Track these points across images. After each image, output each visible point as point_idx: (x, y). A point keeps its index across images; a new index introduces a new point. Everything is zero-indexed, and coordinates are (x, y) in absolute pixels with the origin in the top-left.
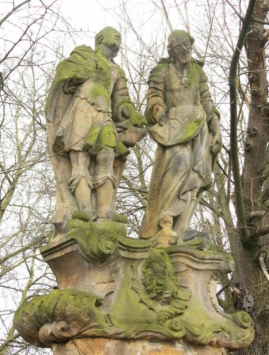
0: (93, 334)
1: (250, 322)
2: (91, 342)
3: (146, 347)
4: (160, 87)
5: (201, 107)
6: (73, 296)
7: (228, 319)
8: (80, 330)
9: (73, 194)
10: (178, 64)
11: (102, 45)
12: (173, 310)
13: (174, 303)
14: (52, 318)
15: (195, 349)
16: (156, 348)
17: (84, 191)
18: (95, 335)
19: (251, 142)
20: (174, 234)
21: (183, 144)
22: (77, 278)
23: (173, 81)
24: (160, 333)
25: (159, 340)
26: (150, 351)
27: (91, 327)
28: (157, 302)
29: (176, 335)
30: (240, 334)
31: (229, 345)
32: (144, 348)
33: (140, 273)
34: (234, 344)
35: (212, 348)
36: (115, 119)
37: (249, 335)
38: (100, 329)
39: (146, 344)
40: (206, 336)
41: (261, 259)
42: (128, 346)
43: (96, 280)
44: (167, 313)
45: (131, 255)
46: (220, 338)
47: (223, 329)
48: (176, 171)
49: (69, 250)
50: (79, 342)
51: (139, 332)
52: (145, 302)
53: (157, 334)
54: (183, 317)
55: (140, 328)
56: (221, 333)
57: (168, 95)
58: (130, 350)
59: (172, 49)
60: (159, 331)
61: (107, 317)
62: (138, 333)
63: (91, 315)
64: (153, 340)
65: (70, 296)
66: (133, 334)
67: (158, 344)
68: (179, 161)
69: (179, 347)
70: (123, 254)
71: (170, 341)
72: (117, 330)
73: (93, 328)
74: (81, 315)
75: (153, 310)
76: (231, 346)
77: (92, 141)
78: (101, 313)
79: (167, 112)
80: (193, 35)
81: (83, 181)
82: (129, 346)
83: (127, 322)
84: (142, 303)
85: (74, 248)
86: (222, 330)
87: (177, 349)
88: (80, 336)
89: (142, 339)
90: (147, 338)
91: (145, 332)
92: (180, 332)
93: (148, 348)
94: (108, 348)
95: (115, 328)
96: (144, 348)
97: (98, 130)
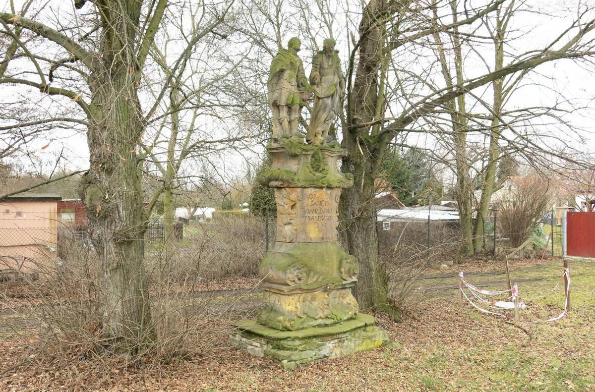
4: (318, 67)
5: (337, 76)
9: (281, 124)
10: (327, 54)
11: (292, 48)
13: (323, 172)
14: (277, 180)
17: (286, 123)
19: (358, 81)
20: (322, 138)
21: (328, 97)
22: (284, 162)
23: (325, 63)
29: (324, 186)
33: (309, 160)
34: (346, 187)
36: (298, 86)
37: (352, 183)
39: (312, 189)
40: (334, 185)
41: (357, 139)
43: (293, 164)
45: (307, 153)
48: (324, 111)
49: (281, 151)
50: (287, 189)
54: (326, 178)
57: (322, 70)
59: (325, 48)
63: (293, 180)
64: (315, 187)
68: (326, 106)
69: (325, 189)
70: (303, 153)
71: (322, 188)
77: (289, 102)
78: (296, 178)
79: (321, 79)
80: (336, 42)
81: (286, 120)
85: (284, 150)
88: (288, 187)
89: (311, 187)
97: (292, 96)
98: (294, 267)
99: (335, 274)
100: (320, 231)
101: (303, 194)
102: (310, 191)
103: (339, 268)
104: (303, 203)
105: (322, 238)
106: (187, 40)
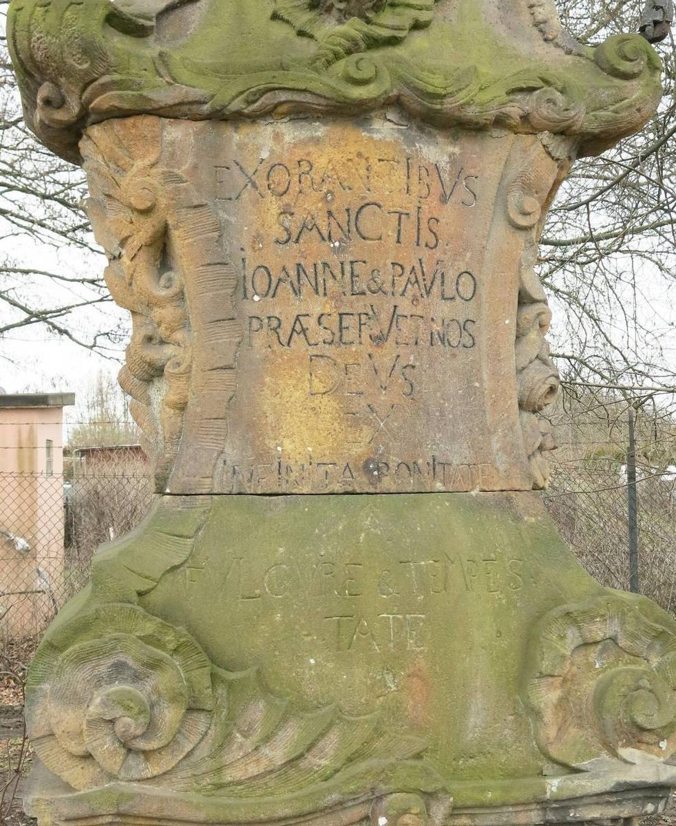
0: (112, 106)
1: (642, 59)
2: (119, 128)
3: (283, 135)
6: (42, 9)
7: (578, 58)
8: (81, 98)
12: (358, 27)
15: (455, 138)
16: (310, 135)
18: (119, 109)
24: (305, 91)
25: (319, 115)
26: (295, 144)
27: (105, 88)
28: (325, 16)
30: (605, 95)
31: (567, 123)
32: (277, 137)
35: (512, 136)
38: (133, 90)
42: (234, 134)
44: (343, 41)
46: (534, 105)
47: (546, 82)
51: (254, 94)
52: (286, 17)
53: (303, 95)
54: (399, 51)
55: (256, 84)
56: (538, 92)
58: (242, 146)
60: (304, 88)
61: (158, 62)
62: (252, 98)
64: (300, 113)
65: (38, 9)
66: (236, 101)
67: (317, 124)
72: (187, 92)
73: (112, 90)
74: (65, 55)
75: (311, 37)
76: (569, 127)
82: (236, 137)
83: (224, 72)
84: (280, 22)
86: (540, 83)
87: (376, 136)
89: (268, 114)
90: (281, 109)
91: (269, 94)
92: (372, 86)
93: (288, 138)
94: (172, 143)
95: (182, 89)
96: (277, 137)
98: (81, 659)
99: (479, 717)
100: (352, 419)
101: (216, 165)
102: (268, 141)
103: (524, 670)
104: (221, 228)
105: (372, 467)
106: (563, 356)
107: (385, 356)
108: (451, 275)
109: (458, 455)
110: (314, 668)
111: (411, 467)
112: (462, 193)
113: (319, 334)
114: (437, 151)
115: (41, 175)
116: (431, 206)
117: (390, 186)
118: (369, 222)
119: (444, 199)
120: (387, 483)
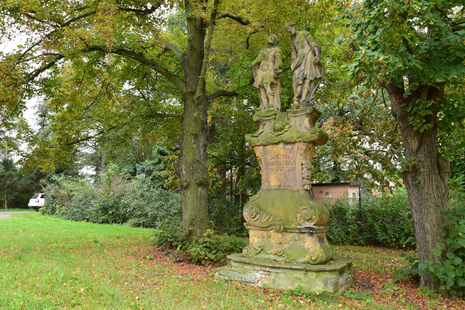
89: (269, 145)
100: (278, 180)
102: (269, 147)
105: (279, 186)
107: (282, 172)
108: (292, 162)
109: (292, 185)
110: (270, 210)
111: (285, 186)
112: (292, 151)
113: (275, 170)
114: (289, 147)
115: (372, 104)
116: (288, 153)
117: (282, 152)
118: (279, 157)
119: (290, 152)
120: (281, 188)
